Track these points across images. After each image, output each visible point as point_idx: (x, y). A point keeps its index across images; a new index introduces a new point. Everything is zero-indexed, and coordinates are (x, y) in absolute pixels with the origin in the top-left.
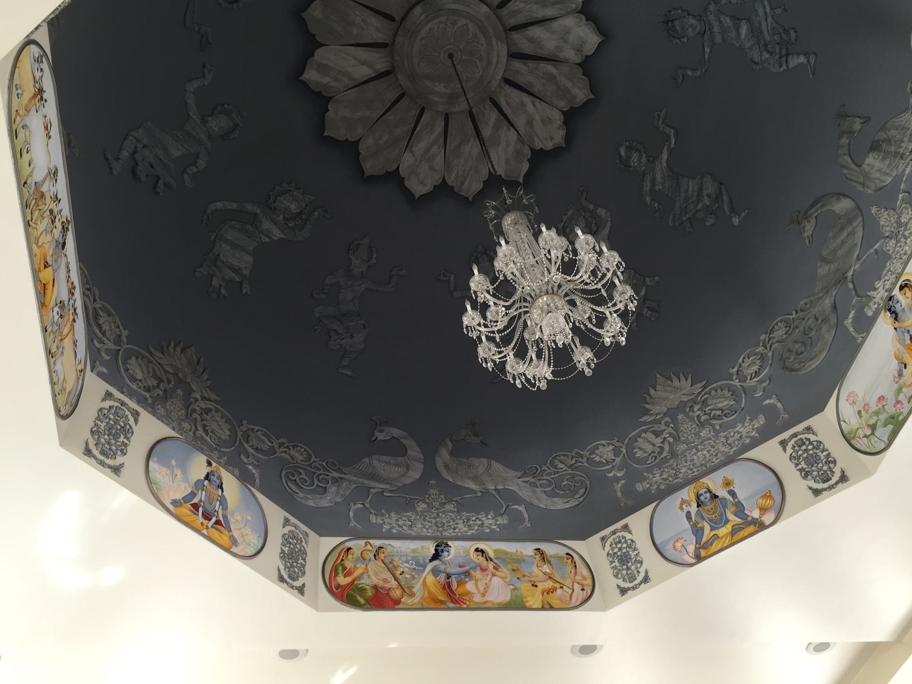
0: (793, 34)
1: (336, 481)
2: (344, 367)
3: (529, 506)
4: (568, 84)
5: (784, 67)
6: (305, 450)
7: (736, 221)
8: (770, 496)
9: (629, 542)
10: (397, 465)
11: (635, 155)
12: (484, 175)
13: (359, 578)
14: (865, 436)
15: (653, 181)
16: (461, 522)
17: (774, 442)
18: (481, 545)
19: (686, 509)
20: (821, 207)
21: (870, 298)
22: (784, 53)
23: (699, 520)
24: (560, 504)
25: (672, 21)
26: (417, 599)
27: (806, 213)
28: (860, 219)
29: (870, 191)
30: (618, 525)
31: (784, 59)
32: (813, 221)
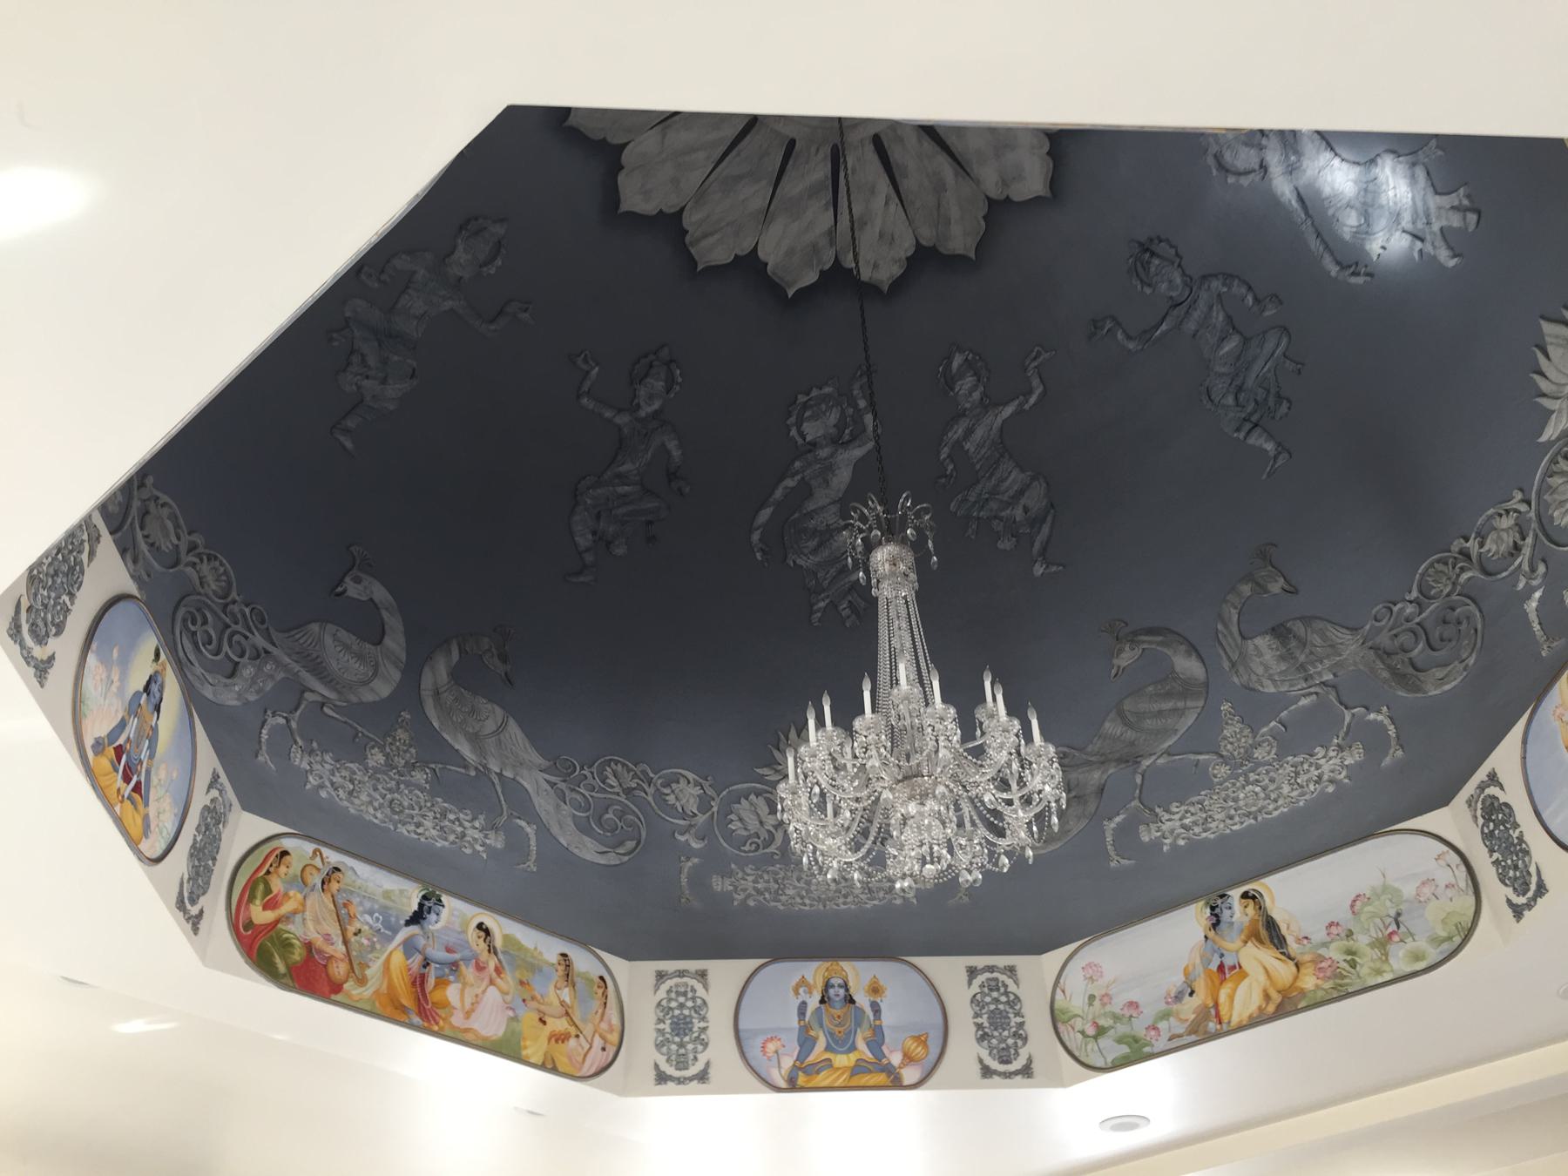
0: (1284, 408)
1: (258, 655)
2: (347, 431)
3: (543, 830)
4: (955, 212)
5: (1242, 435)
6: (225, 573)
7: (1039, 570)
8: (924, 1043)
9: (699, 1002)
10: (360, 657)
11: (969, 381)
12: (745, 247)
13: (287, 918)
14: (1083, 1033)
15: (969, 432)
16: (431, 814)
17: (961, 963)
18: (490, 920)
19: (803, 996)
20: (1159, 644)
21: (1157, 819)
22: (1254, 418)
23: (815, 1025)
24: (588, 850)
25: (1153, 254)
26: (367, 992)
27: (1135, 633)
28: (1201, 703)
29: (1236, 680)
30: (693, 965)
31: (1248, 426)
32: (1137, 652)
